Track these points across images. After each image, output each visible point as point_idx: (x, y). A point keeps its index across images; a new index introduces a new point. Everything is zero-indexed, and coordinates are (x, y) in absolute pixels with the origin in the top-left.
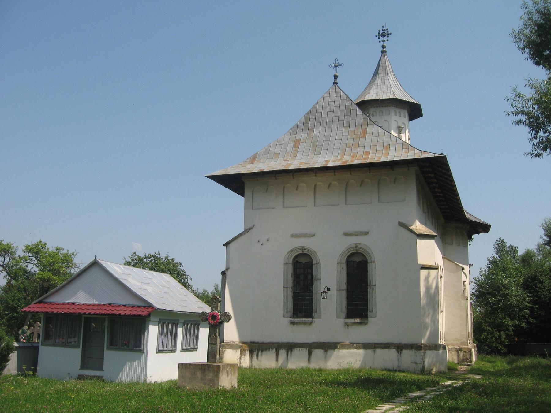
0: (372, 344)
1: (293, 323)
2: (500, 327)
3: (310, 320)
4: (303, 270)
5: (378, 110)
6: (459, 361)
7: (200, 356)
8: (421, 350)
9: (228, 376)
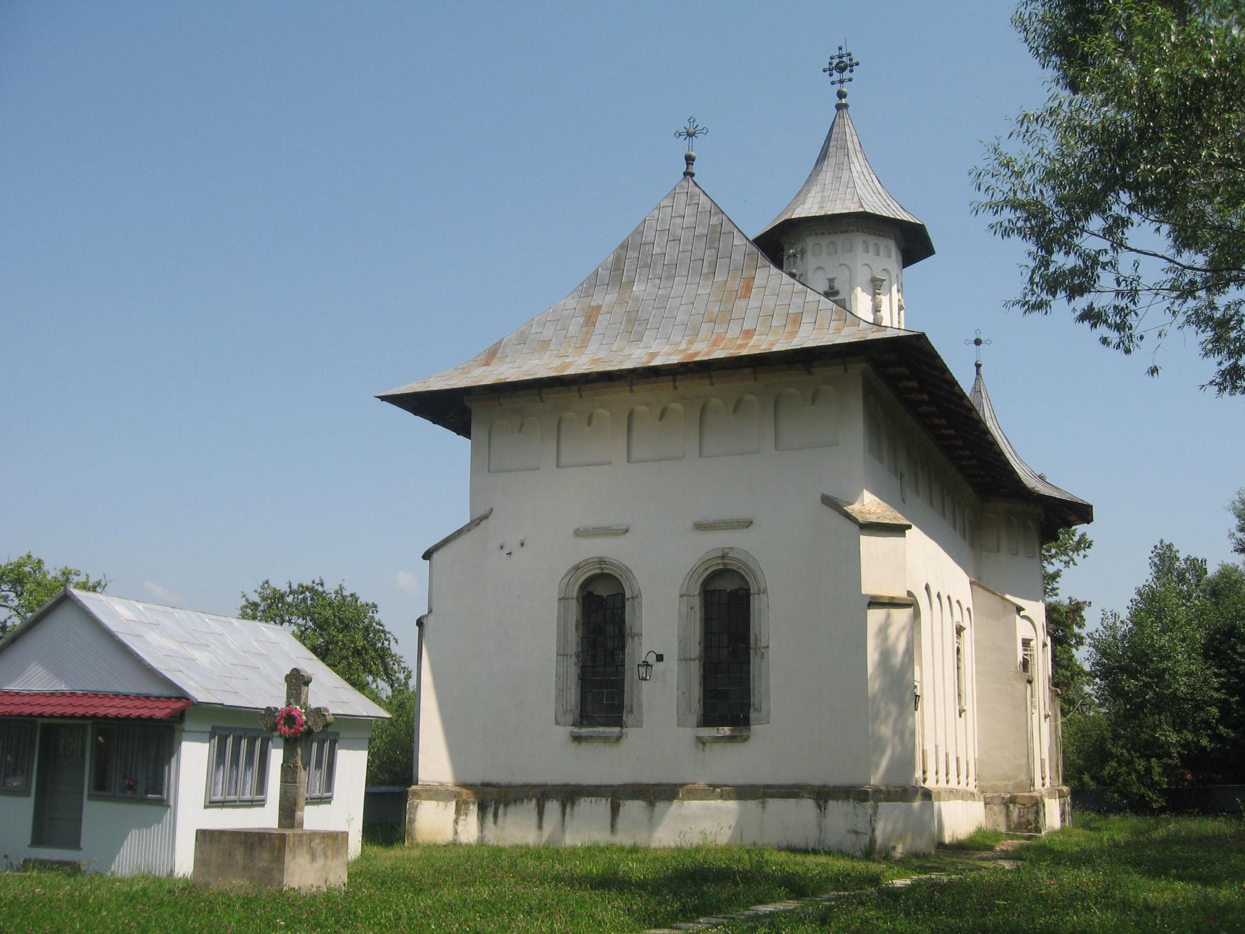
0: (759, 786)
1: (577, 739)
2: (1152, 749)
3: (616, 730)
4: (601, 612)
5: (824, 241)
6: (1009, 827)
7: (265, 818)
8: (866, 800)
9: (313, 859)
